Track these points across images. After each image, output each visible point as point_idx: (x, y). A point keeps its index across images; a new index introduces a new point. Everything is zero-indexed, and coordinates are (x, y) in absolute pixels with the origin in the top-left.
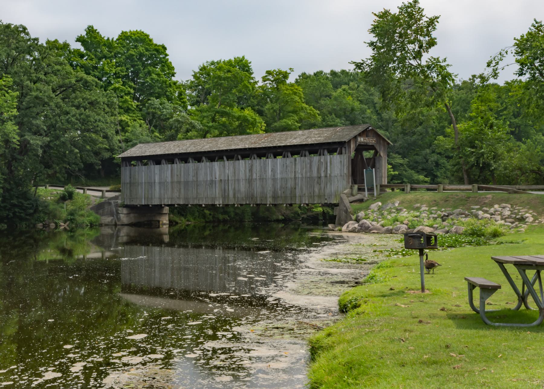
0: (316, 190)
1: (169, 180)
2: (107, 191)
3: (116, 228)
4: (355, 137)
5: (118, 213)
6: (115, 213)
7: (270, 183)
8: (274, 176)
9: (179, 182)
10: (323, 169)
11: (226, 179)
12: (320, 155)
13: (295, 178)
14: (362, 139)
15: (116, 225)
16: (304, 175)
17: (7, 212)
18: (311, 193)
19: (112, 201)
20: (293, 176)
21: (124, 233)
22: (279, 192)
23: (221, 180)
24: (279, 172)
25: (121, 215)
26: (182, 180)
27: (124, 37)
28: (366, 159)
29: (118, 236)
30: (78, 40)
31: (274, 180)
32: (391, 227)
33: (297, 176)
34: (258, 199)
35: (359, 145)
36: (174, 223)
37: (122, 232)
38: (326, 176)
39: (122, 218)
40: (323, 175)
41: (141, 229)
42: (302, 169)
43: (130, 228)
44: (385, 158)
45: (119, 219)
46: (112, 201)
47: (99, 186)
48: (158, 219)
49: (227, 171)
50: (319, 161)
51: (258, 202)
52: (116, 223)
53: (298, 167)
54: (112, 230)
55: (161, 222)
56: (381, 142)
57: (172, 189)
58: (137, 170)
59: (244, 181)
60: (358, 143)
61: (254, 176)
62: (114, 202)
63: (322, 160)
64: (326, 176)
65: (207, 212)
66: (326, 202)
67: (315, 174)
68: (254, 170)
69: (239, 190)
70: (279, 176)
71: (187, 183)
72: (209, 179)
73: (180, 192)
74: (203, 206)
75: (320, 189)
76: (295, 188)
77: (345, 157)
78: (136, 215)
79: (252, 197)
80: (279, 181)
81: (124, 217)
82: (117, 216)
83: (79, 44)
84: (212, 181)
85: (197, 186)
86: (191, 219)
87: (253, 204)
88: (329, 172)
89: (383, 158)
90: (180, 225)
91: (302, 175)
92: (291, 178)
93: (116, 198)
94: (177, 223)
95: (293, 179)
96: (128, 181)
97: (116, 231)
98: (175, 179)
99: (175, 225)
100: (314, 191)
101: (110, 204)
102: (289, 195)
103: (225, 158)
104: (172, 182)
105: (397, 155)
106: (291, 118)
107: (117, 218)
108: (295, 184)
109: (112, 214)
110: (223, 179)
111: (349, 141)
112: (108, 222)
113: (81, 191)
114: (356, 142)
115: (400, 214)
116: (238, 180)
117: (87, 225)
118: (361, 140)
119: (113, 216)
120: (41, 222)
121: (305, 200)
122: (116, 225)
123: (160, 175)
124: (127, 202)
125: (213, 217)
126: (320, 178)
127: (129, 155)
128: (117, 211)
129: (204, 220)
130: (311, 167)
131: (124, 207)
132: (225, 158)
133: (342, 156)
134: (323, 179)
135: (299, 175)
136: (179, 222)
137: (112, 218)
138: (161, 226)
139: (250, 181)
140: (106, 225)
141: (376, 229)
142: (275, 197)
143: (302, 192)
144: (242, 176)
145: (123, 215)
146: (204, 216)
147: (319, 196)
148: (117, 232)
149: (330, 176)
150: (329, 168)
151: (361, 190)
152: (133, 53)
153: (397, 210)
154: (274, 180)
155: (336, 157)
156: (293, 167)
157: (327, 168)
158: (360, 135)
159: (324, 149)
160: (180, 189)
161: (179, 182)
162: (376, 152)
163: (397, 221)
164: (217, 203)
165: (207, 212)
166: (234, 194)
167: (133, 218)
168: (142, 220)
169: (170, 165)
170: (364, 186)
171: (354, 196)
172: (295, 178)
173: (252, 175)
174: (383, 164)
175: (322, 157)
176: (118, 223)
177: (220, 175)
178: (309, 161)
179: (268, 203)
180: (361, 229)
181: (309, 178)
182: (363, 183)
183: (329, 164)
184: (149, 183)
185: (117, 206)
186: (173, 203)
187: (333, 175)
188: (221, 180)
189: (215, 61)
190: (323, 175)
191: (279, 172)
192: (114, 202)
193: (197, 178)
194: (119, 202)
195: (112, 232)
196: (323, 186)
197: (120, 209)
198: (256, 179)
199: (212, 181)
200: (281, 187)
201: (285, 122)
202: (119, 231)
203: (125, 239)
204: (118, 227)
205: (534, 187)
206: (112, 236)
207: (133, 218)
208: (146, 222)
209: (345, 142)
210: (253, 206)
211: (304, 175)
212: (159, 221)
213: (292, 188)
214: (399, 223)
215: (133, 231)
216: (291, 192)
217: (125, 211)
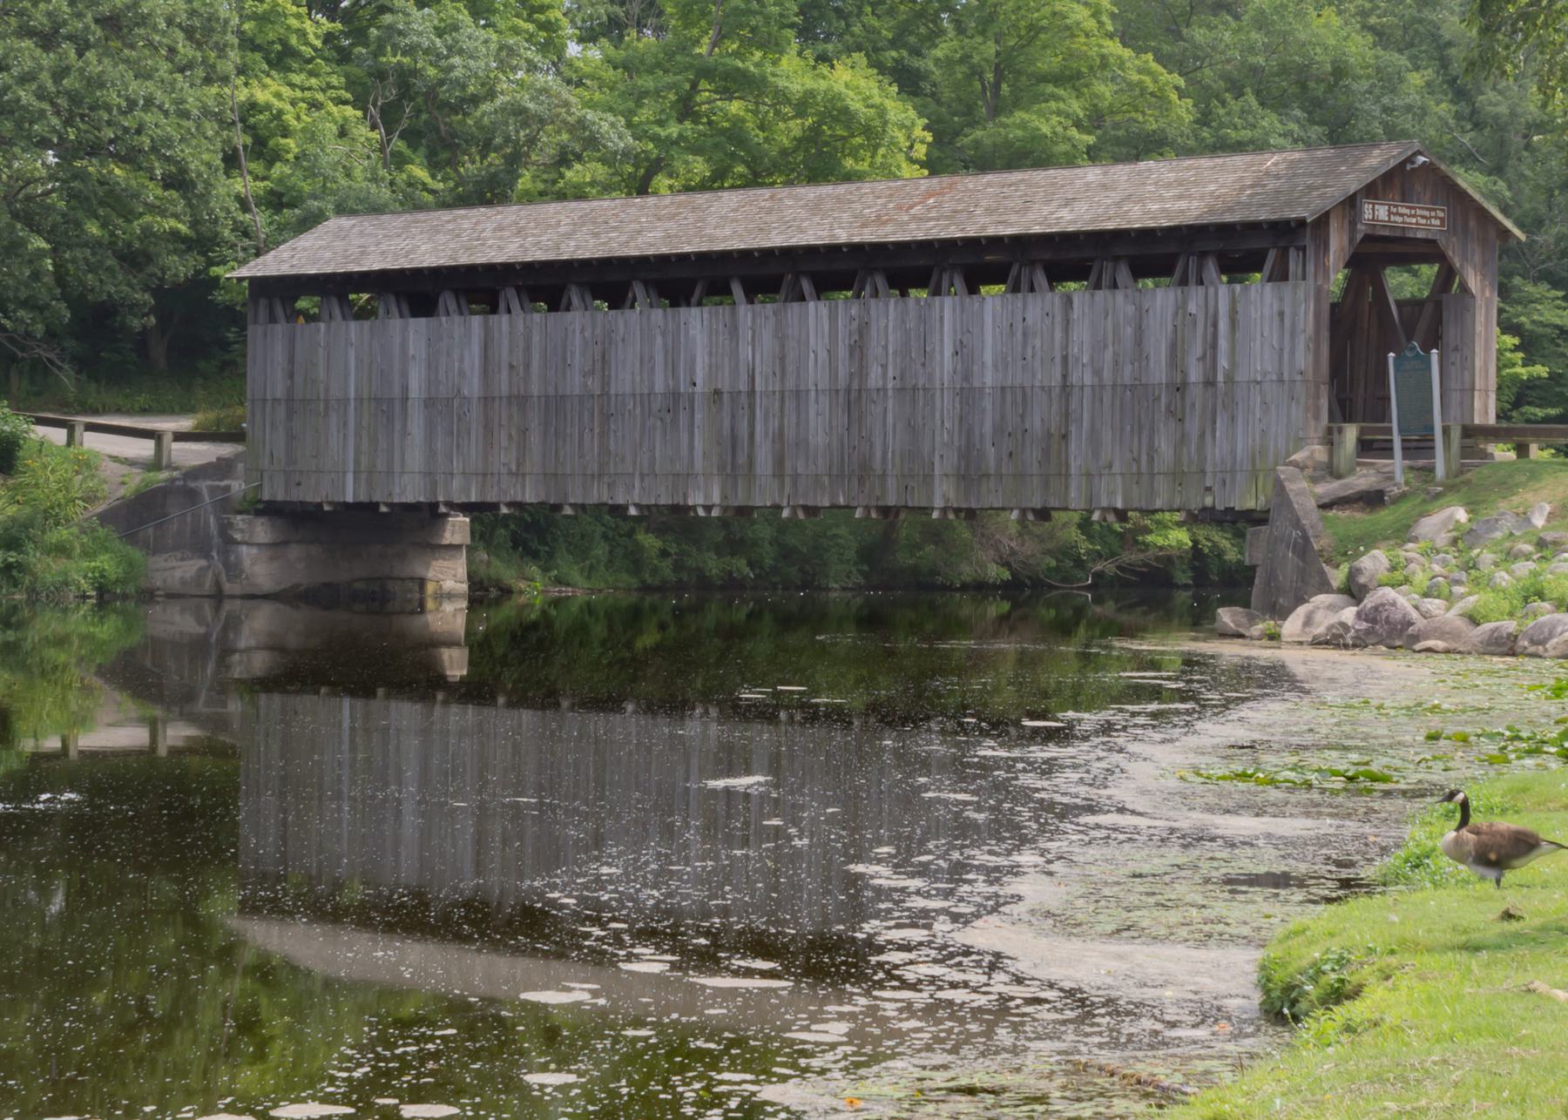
0: (1165, 446)
3: (217, 609)
4: (1351, 203)
6: (216, 540)
7: (946, 407)
8: (967, 377)
9: (520, 401)
10: (1197, 349)
11: (743, 386)
13: (1066, 388)
14: (1382, 212)
15: (218, 597)
16: (1107, 375)
18: (1137, 460)
20: (1056, 380)
24: (988, 357)
25: (244, 549)
26: (535, 389)
28: (1399, 304)
29: (226, 651)
31: (968, 395)
32: (1510, 626)
33: (1074, 378)
35: (1369, 239)
36: (494, 593)
37: (245, 630)
38: (1210, 383)
39: (247, 563)
40: (1195, 374)
44: (1488, 303)
45: (233, 570)
46: (203, 485)
47: (144, 411)
48: (418, 570)
49: (746, 351)
50: (1181, 307)
51: (891, 500)
52: (218, 584)
53: (1082, 333)
54: (200, 620)
55: (430, 588)
56: (1472, 223)
59: (825, 401)
60: (1361, 229)
61: (874, 378)
62: (212, 490)
63: (1192, 308)
64: (1210, 383)
65: (649, 541)
66: (1208, 501)
67: (1159, 372)
68: (874, 350)
71: (555, 405)
72: (659, 387)
73: (523, 448)
74: (326, 508)
75: (1182, 441)
76: (1065, 437)
77: (1301, 294)
80: (987, 404)
84: (675, 396)
85: (606, 417)
86: (576, 575)
87: (867, 508)
88: (1223, 363)
89: (1479, 302)
91: (1097, 373)
92: (1047, 390)
94: (507, 592)
95: (1056, 393)
97: (219, 627)
98: (503, 385)
99: (497, 602)
100: (1152, 451)
101: (192, 496)
104: (487, 400)
105: (1542, 289)
106: (1053, 105)
107: (226, 565)
108: (1067, 415)
110: (725, 387)
111: (1323, 221)
112: (183, 582)
113: (58, 436)
114: (1353, 224)
115: (1554, 564)
116: (799, 394)
118: (1378, 213)
119: (207, 556)
121: (1112, 493)
122: (218, 597)
123: (432, 365)
124: (275, 491)
125: (678, 567)
126: (1180, 388)
127: (286, 270)
128: (225, 528)
131: (258, 513)
133: (1287, 288)
134: (1196, 393)
135: (1083, 376)
137: (203, 563)
138: (430, 604)
140: (172, 596)
141: (1441, 634)
144: (815, 375)
145: (254, 551)
146: (635, 561)
148: (225, 629)
149: (1230, 379)
150: (1223, 344)
151: (1367, 447)
153: (1541, 544)
154: (968, 395)
156: (1058, 334)
158: (1373, 190)
159: (1203, 255)
161: (520, 401)
162: (1448, 275)
163: (1541, 595)
164: (696, 499)
165: (649, 541)
166: (779, 462)
169: (476, 321)
171: (1339, 477)
172: (1066, 388)
173: (862, 372)
174: (1479, 328)
176: (228, 587)
178: (1131, 309)
179: (938, 503)
180: (1368, 632)
181: (1133, 388)
182: (1384, 415)
183: (1223, 326)
184: (378, 401)
185: (225, 505)
187: (1241, 377)
188: (717, 393)
190: (1195, 374)
191: (988, 357)
192: (212, 490)
193: (605, 383)
194: (237, 486)
195: (202, 630)
196: (1193, 426)
199: (675, 396)
200: (999, 429)
201: (1023, 125)
202: (232, 624)
203: (260, 663)
204: (227, 606)
206: (197, 648)
208: (359, 586)
209: (1301, 223)
211: (1107, 375)
212: (422, 582)
213: (1049, 435)
214: (1547, 605)
215: (296, 625)
216: (1046, 452)
217: (262, 531)
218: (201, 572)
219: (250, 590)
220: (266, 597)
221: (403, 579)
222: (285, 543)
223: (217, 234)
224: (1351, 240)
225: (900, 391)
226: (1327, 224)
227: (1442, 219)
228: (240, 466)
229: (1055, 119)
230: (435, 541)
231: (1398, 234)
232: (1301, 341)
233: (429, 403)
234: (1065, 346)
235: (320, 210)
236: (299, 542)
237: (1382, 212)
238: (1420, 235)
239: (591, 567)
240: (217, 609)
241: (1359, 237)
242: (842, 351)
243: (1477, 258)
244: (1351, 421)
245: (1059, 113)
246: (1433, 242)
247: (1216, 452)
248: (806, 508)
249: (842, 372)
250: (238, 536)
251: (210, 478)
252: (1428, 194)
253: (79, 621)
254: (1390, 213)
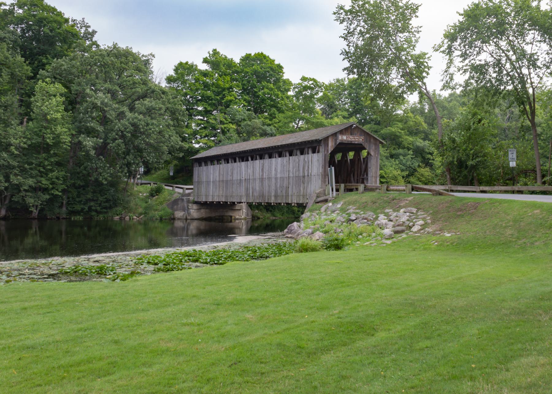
0: (302, 189)
1: (218, 179)
2: (187, 189)
3: (186, 221)
4: (335, 135)
5: (188, 209)
8: (276, 175)
9: (223, 181)
12: (305, 154)
14: (345, 138)
15: (186, 219)
17: (82, 206)
19: (185, 198)
21: (193, 227)
22: (279, 191)
23: (245, 179)
24: (279, 171)
25: (191, 210)
27: (247, 59)
29: (188, 229)
30: (205, 61)
31: (276, 179)
33: (290, 175)
34: (266, 197)
35: (340, 144)
36: (256, 218)
38: (308, 176)
39: (192, 213)
40: (306, 174)
41: (213, 223)
42: (293, 168)
43: (200, 222)
45: (189, 214)
46: (185, 198)
49: (249, 170)
50: (304, 159)
51: (266, 201)
55: (233, 218)
56: (372, 140)
57: (219, 188)
58: (212, 172)
60: (338, 142)
61: (264, 177)
64: (308, 176)
68: (265, 170)
69: (255, 189)
70: (279, 176)
71: (227, 181)
72: (239, 179)
74: (229, 203)
75: (304, 189)
76: (289, 187)
78: (207, 210)
79: (263, 196)
81: (194, 211)
82: (188, 211)
83: (205, 64)
84: (240, 180)
85: (233, 184)
87: (284, 203)
88: (310, 171)
90: (261, 220)
91: (293, 174)
92: (286, 177)
93: (189, 195)
94: (259, 218)
96: (197, 180)
98: (221, 179)
101: (183, 200)
102: (284, 195)
103: (250, 159)
104: (219, 181)
107: (188, 213)
109: (184, 210)
111: (326, 139)
112: (181, 216)
113: (171, 188)
114: (336, 140)
117: (157, 219)
118: (343, 138)
119: (185, 212)
120: (117, 215)
122: (186, 219)
126: (304, 177)
127: (201, 156)
128: (188, 206)
129: (293, 216)
130: (299, 167)
131: (194, 203)
132: (250, 159)
133: (319, 154)
134: (306, 177)
135: (291, 175)
136: (261, 217)
138: (233, 221)
139: (262, 180)
140: (178, 219)
142: (276, 196)
143: (293, 192)
144: (257, 176)
145: (193, 210)
147: (303, 196)
148: (188, 225)
149: (311, 175)
152: (248, 71)
154: (276, 179)
155: (315, 155)
157: (309, 168)
158: (341, 132)
159: (308, 148)
160: (223, 187)
167: (203, 213)
168: (213, 215)
170: (336, 186)
171: (326, 196)
173: (263, 175)
175: (306, 155)
176: (188, 218)
177: (245, 174)
178: (298, 160)
184: (207, 182)
185: (189, 201)
186: (219, 201)
189: (340, 79)
190: (306, 174)
191: (279, 171)
194: (191, 198)
196: (306, 185)
197: (190, 205)
198: (265, 178)
199: (240, 180)
200: (280, 186)
201: (389, 130)
202: (189, 224)
203: (194, 232)
204: (188, 221)
205: (460, 188)
206: (183, 228)
207: (203, 213)
208: (217, 217)
210: (284, 205)
212: (231, 217)
215: (203, 225)
216: (286, 191)
217: (195, 207)
218: (184, 214)
219: (192, 218)
220: (196, 219)
221: (227, 216)
222: (200, 209)
223: (10, 142)
224: (335, 144)
225: (268, 178)
226: (328, 140)
227: (363, 139)
228: (192, 194)
229: (396, 128)
230: (234, 209)
231: (350, 142)
232: (321, 165)
233: (213, 182)
234: (289, 168)
235: (182, 142)
236: (204, 209)
237: (345, 138)
238: (356, 143)
239: (283, 214)
240: (186, 221)
241: (338, 143)
242: (261, 170)
243: (373, 148)
244: (343, 183)
245: (397, 127)
246: (361, 144)
247: (309, 191)
248: (286, 203)
249: (261, 174)
250: (190, 208)
251: (186, 196)
252: (359, 134)
253: (157, 224)
254: (347, 138)
